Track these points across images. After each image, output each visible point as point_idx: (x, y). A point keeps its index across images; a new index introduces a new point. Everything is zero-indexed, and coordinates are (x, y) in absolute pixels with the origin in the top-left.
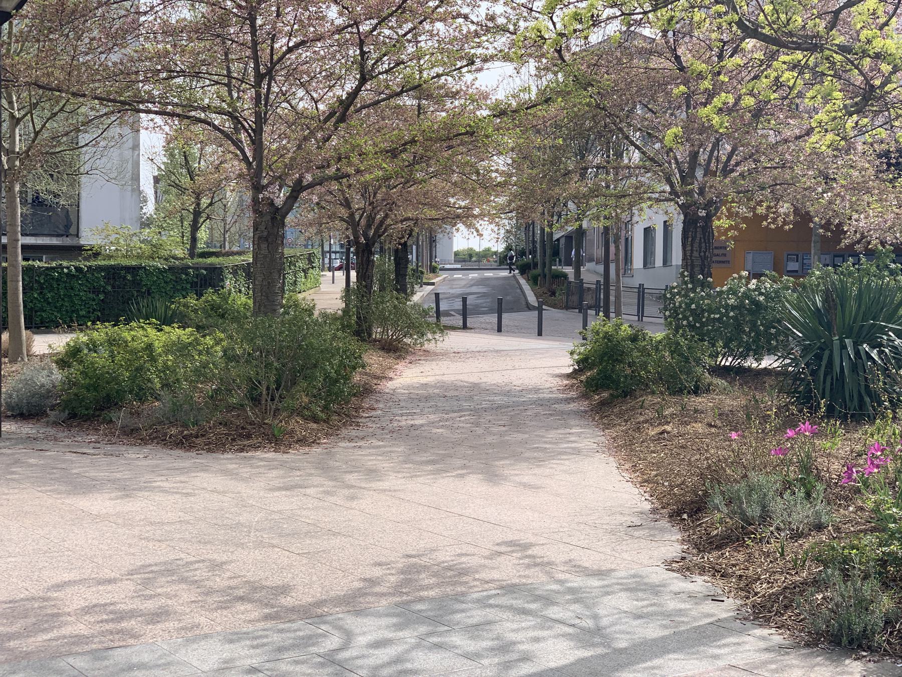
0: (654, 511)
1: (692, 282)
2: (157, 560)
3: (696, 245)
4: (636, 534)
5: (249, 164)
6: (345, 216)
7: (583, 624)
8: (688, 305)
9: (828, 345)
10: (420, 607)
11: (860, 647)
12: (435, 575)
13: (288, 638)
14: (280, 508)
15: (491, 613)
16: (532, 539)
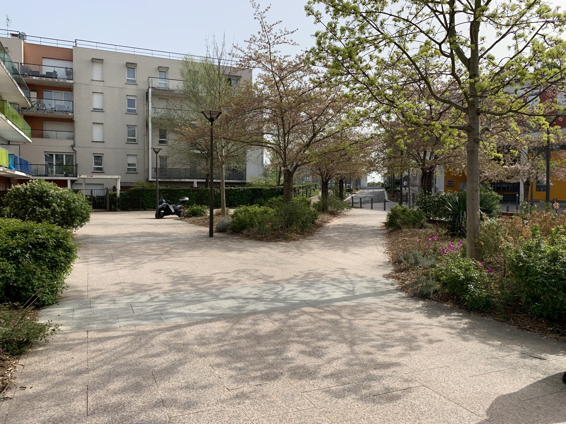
0: (389, 262)
1: (424, 193)
2: (242, 268)
3: (426, 182)
4: (380, 268)
5: (283, 159)
6: (320, 173)
7: (350, 289)
8: (422, 201)
9: (459, 214)
10: (305, 283)
11: (427, 298)
12: (315, 275)
13: (268, 288)
14: (280, 257)
15: (324, 285)
16: (347, 267)
